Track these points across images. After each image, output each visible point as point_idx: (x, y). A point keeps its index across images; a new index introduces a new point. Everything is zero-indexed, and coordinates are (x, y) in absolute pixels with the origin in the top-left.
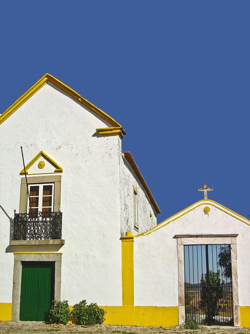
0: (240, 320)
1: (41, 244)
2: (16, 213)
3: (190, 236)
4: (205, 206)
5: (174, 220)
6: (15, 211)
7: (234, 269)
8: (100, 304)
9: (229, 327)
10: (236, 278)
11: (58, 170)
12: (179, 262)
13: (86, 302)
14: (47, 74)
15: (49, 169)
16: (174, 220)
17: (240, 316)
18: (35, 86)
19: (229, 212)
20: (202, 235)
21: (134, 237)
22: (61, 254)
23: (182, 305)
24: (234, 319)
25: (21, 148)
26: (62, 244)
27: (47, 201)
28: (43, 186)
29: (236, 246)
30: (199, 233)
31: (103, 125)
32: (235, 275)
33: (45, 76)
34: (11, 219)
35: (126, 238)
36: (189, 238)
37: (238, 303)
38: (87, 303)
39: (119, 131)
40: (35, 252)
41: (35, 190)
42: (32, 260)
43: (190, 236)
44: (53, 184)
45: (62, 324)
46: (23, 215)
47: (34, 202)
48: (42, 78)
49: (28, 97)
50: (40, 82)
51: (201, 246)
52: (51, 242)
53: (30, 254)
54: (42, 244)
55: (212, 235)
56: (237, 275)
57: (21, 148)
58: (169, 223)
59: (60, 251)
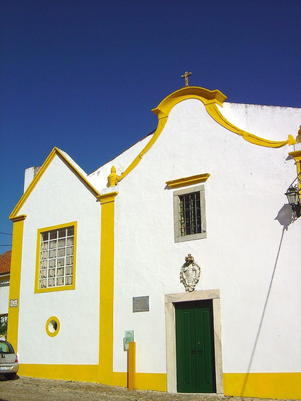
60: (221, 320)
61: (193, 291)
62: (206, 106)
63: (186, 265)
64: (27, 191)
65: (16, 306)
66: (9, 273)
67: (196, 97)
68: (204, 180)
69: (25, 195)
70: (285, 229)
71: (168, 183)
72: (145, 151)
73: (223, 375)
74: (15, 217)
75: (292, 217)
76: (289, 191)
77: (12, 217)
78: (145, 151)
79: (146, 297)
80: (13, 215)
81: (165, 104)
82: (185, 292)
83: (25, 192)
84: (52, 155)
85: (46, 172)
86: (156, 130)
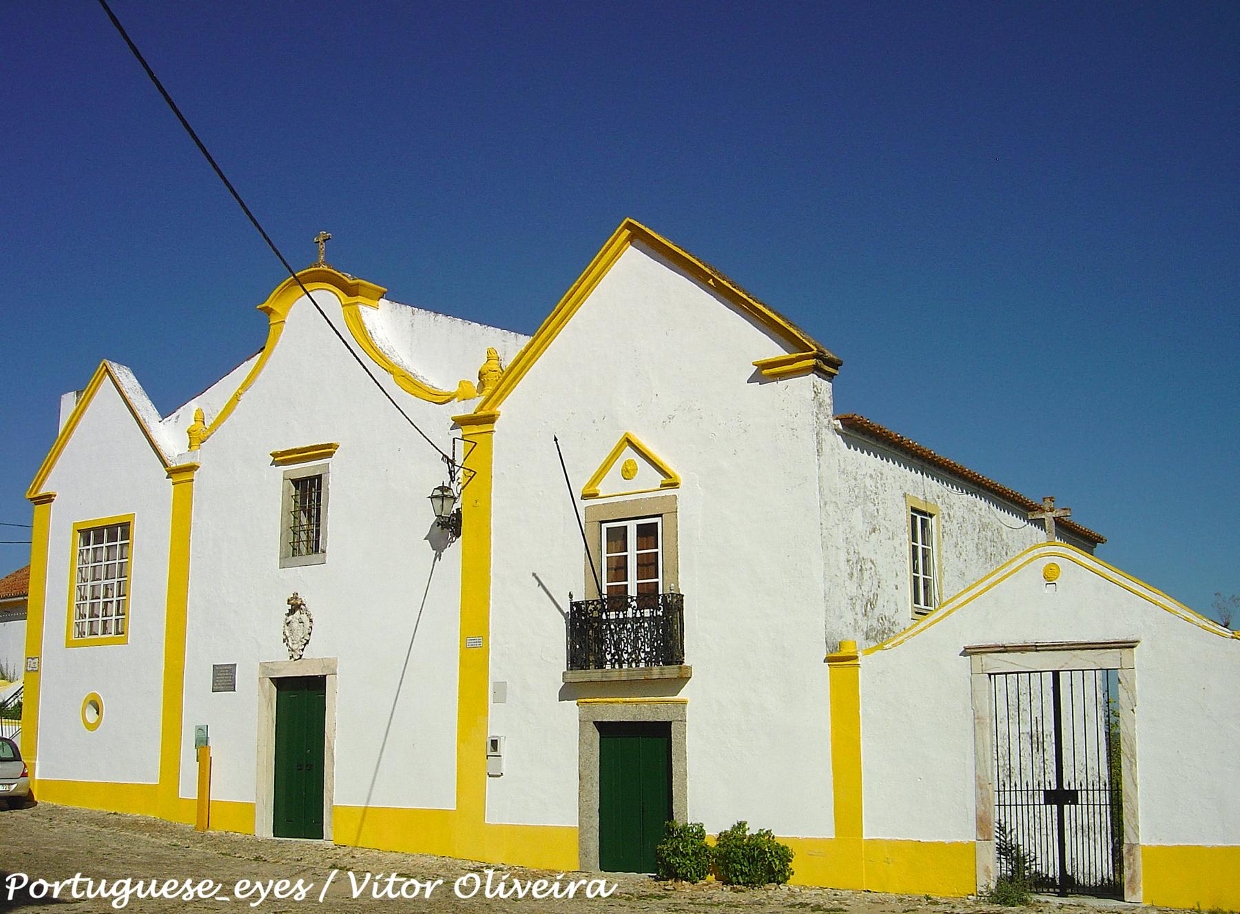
0: (1141, 886)
1: (633, 678)
2: (574, 600)
3: (1004, 649)
4: (1048, 560)
5: (963, 604)
6: (571, 596)
7: (1126, 739)
8: (781, 835)
9: (1112, 904)
10: (1131, 766)
11: (669, 481)
12: (976, 721)
13: (747, 827)
14: (628, 219)
15: (648, 479)
16: (963, 604)
17: (1141, 874)
18: (602, 256)
19: (1115, 576)
20: (1037, 646)
21: (860, 654)
22: (684, 703)
23: (986, 838)
24: (1126, 881)
25: (556, 440)
26: (683, 679)
27: (648, 565)
28: (637, 525)
29: (1134, 675)
30: (1030, 640)
31: (773, 350)
32: (1129, 756)
33: (622, 225)
34: (565, 615)
35: (839, 659)
36: (1001, 654)
37: (1138, 837)
38: (749, 829)
39: (812, 362)
40: (624, 699)
41: (618, 537)
42: (618, 720)
43: (1004, 649)
44: (658, 520)
45: (686, 881)
46: (589, 604)
47: (651, 564)
48: (617, 231)
49: (589, 288)
50: (613, 243)
51: (1004, 675)
52: (656, 672)
53: (612, 702)
54: (636, 678)
55: (1064, 645)
56: (1133, 756)
57: (556, 440)
58: (949, 612)
59: (680, 696)
60: (336, 714)
61: (300, 658)
62: (345, 307)
63: (292, 612)
64: (63, 434)
65: (36, 669)
66: (27, 595)
67: (331, 289)
68: (330, 455)
69: (61, 438)
70: (438, 559)
71: (274, 455)
72: (245, 386)
73: (332, 807)
74: (35, 496)
75: (450, 537)
76: (438, 493)
77: (32, 494)
78: (245, 386)
79: (232, 665)
80: (34, 491)
81: (279, 297)
82: (289, 659)
83: (60, 433)
84: (93, 387)
85: (81, 422)
86: (264, 348)
